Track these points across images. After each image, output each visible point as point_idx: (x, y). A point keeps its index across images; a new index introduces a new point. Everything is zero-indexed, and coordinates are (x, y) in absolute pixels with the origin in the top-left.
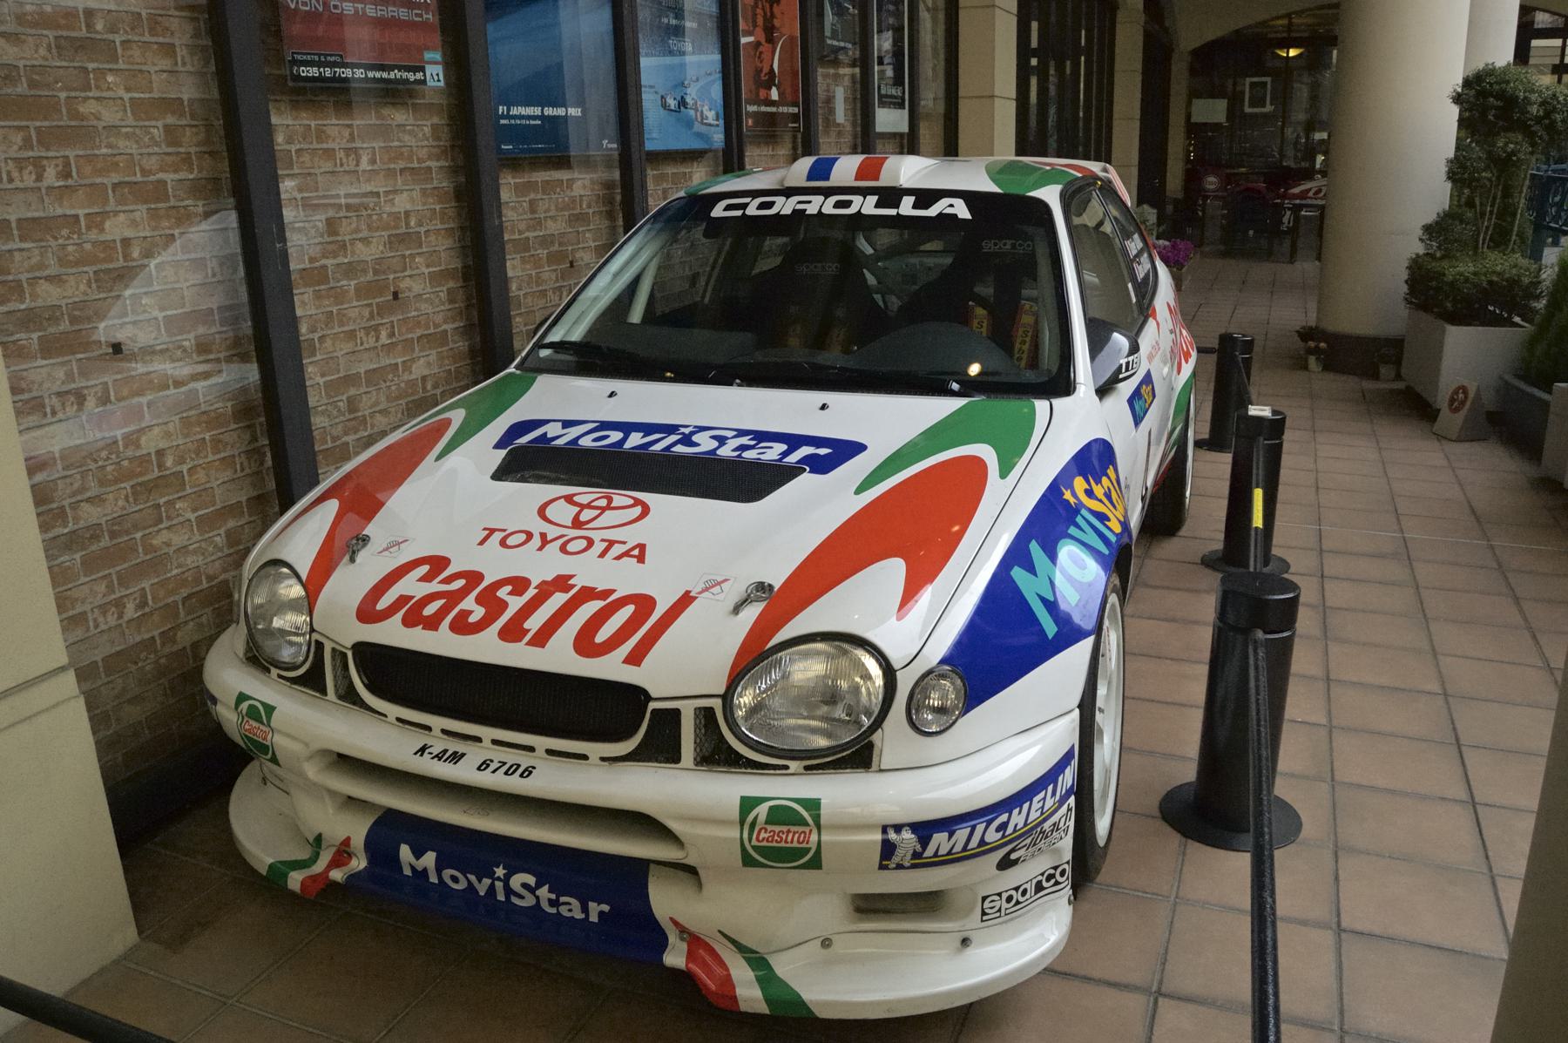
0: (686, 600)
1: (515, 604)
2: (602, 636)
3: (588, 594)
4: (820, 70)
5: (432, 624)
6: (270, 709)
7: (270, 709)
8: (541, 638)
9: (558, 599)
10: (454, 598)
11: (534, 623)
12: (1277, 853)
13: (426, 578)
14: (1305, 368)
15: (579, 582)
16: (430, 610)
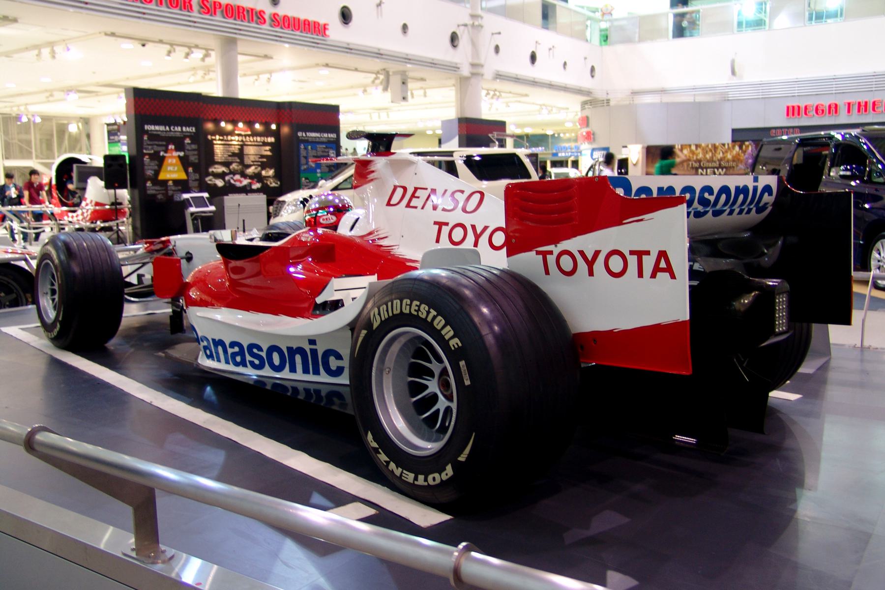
0: (416, 207)
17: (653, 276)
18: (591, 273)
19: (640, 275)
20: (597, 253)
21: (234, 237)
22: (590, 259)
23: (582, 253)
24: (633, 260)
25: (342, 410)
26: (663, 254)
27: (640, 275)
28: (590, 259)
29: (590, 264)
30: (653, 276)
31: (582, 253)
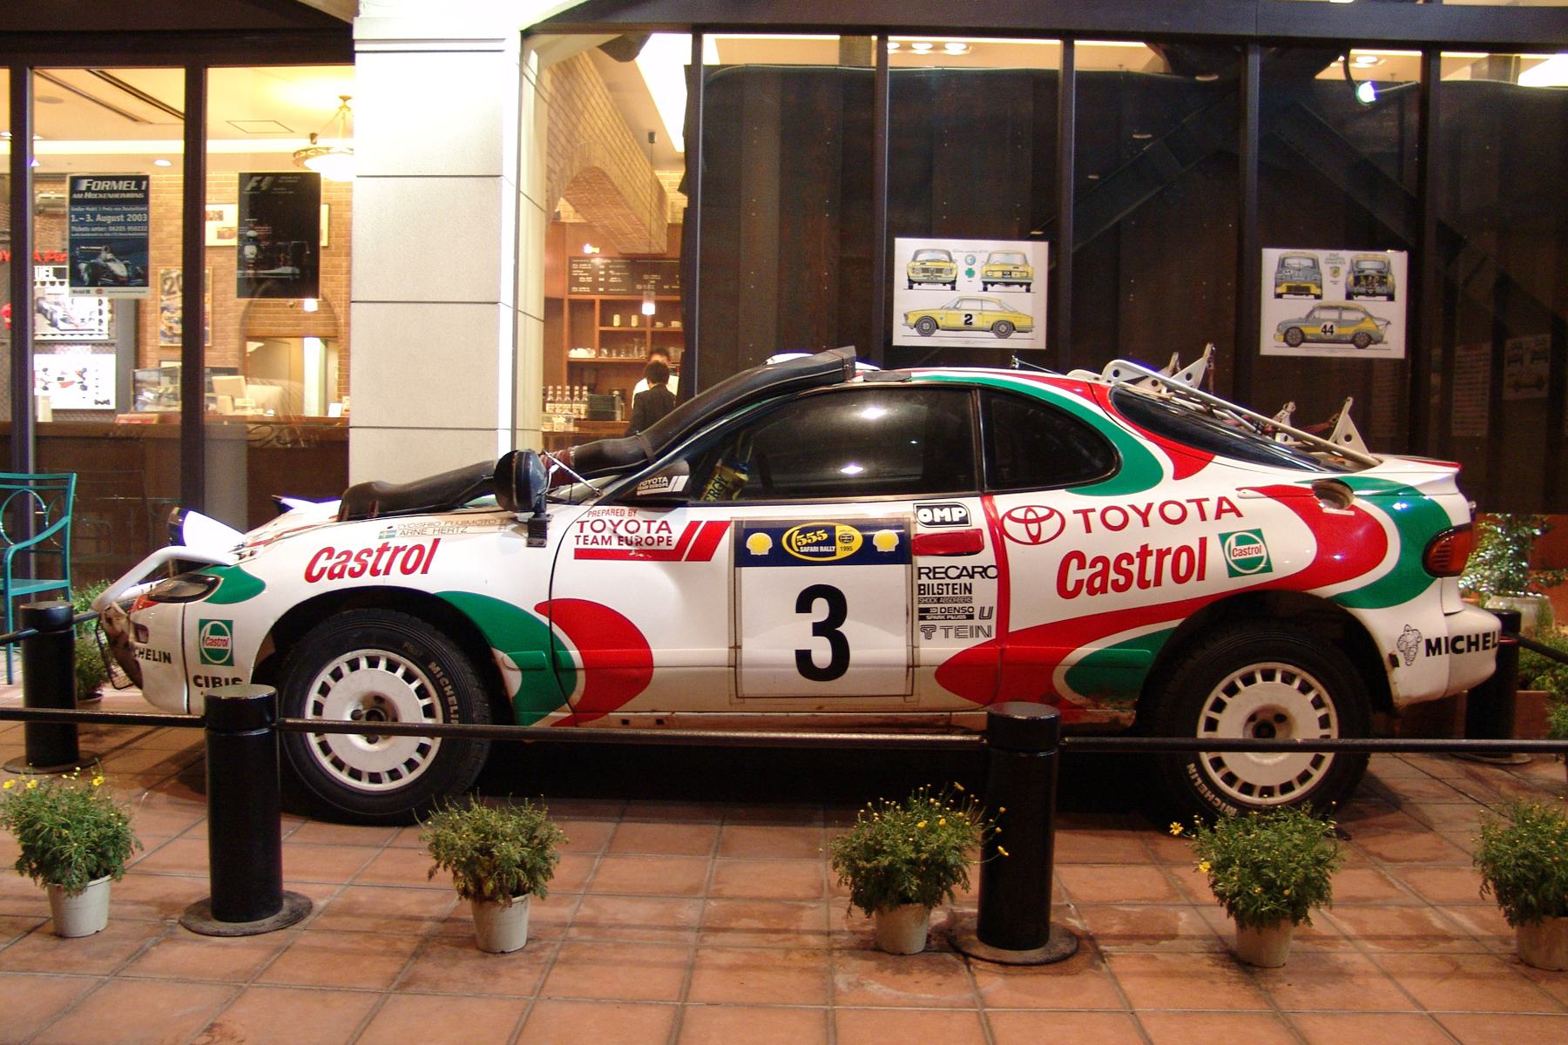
0: (436, 542)
1: (371, 561)
2: (409, 566)
3: (397, 550)
4: (1271, 257)
5: (341, 575)
6: (229, 624)
7: (229, 624)
8: (387, 572)
9: (387, 556)
10: (1104, 574)
11: (382, 566)
12: (1454, 524)
13: (329, 558)
14: (1390, 801)
15: (1153, 547)
16: (337, 571)
17: (1218, 517)
18: (1146, 524)
19: (1203, 518)
20: (1149, 506)
21: (671, 163)
22: (1012, 629)
23: (1133, 507)
24: (1192, 509)
25: (179, 374)
26: (1221, 500)
27: (1203, 518)
28: (1012, 629)
29: (1144, 516)
30: (1218, 517)
31: (1133, 507)
